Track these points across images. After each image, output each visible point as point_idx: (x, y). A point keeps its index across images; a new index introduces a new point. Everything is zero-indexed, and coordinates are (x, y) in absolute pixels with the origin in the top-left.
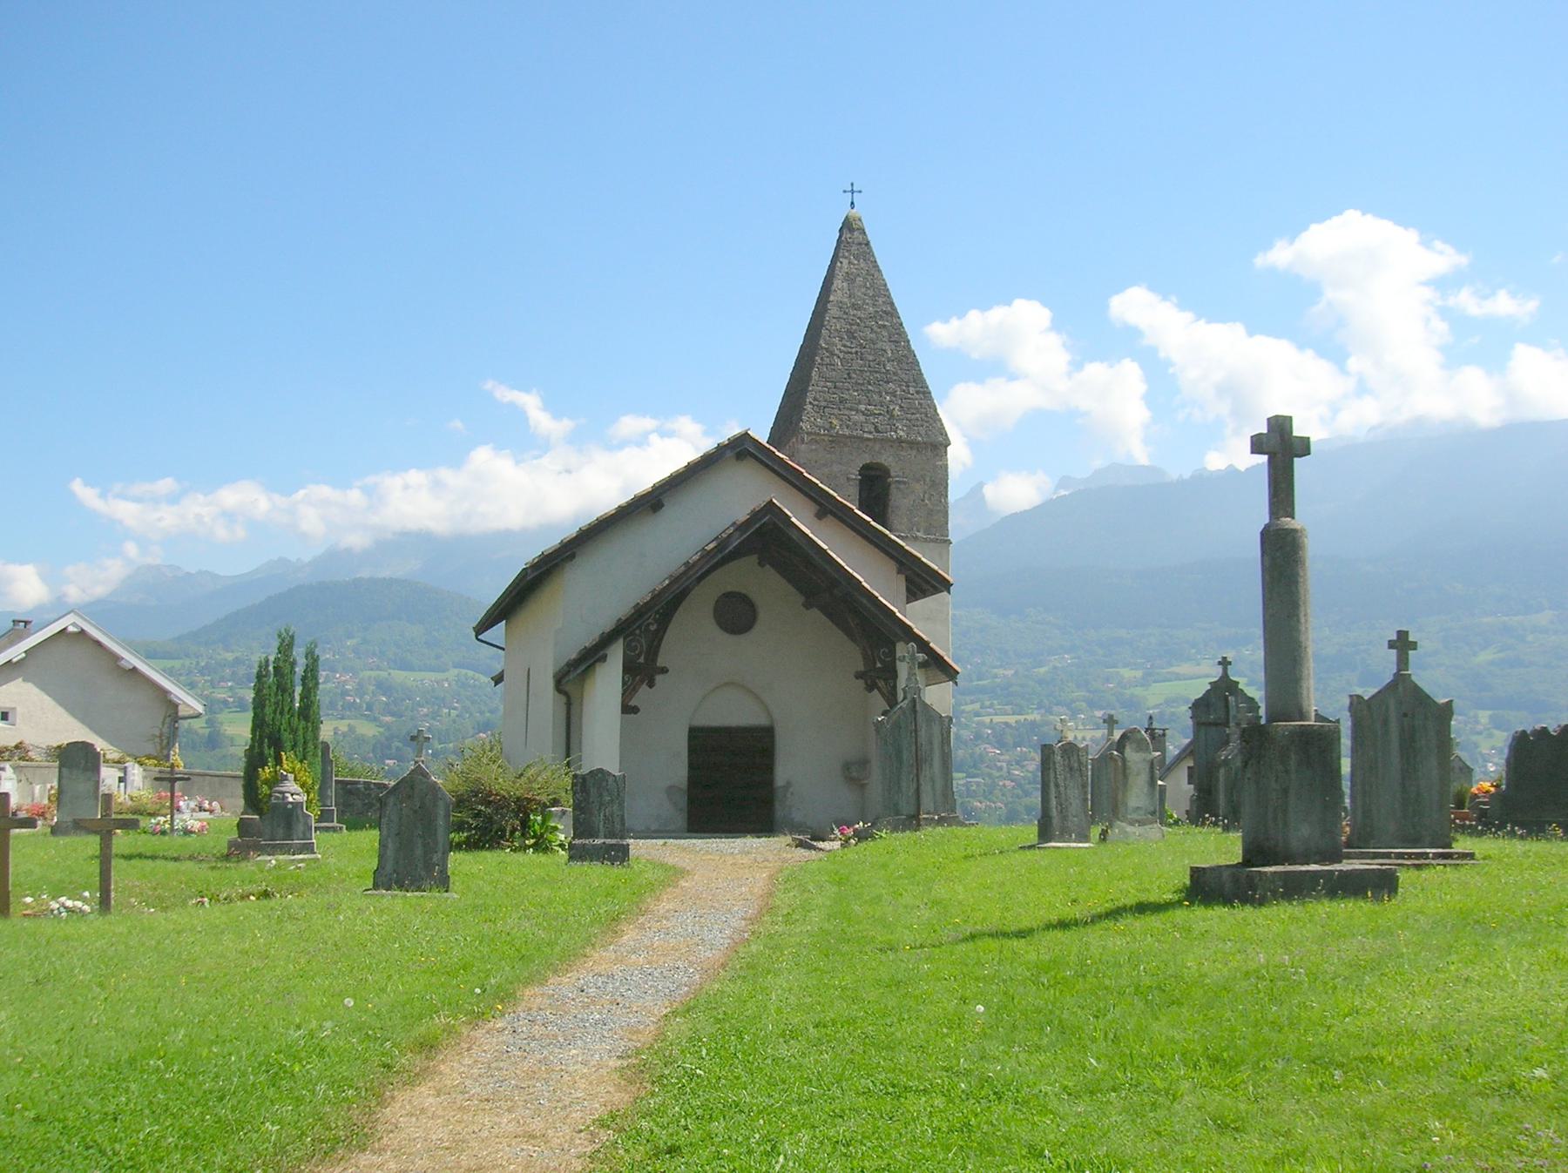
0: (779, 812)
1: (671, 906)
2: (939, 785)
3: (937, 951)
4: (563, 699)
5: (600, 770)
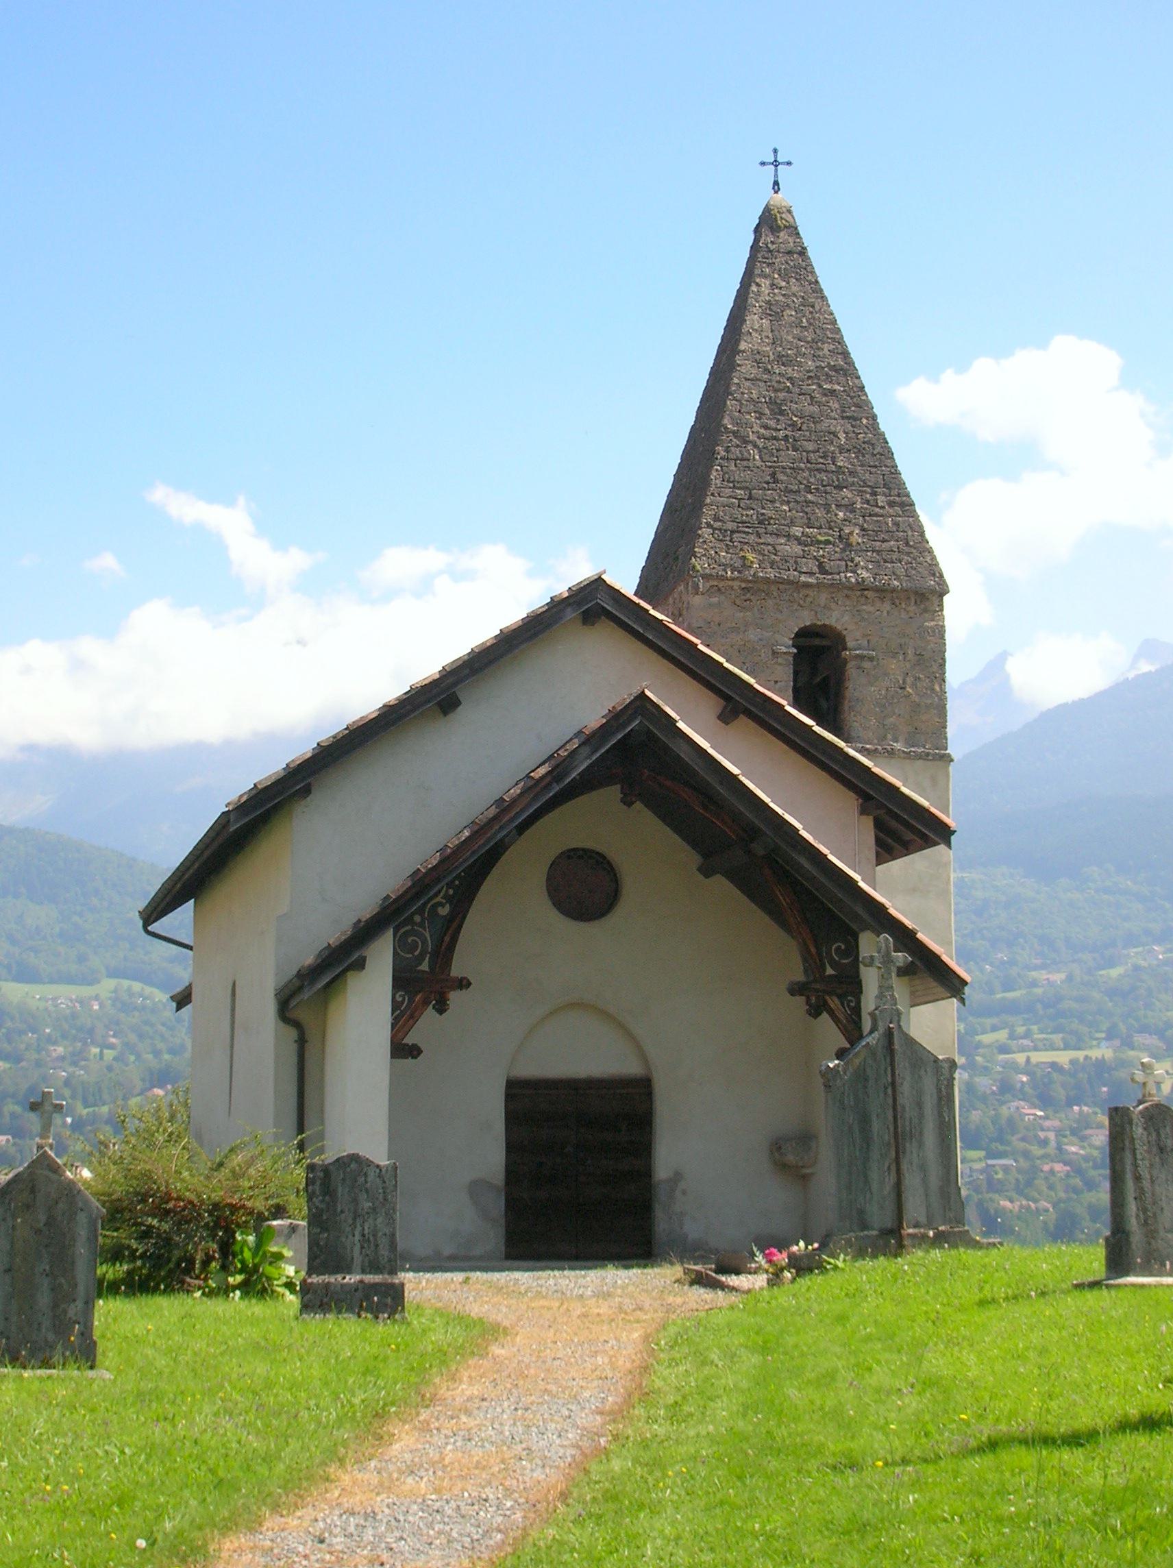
0: (661, 1224)
1: (475, 1390)
2: (934, 1182)
3: (931, 1469)
4: (292, 1033)
5: (354, 1158)
